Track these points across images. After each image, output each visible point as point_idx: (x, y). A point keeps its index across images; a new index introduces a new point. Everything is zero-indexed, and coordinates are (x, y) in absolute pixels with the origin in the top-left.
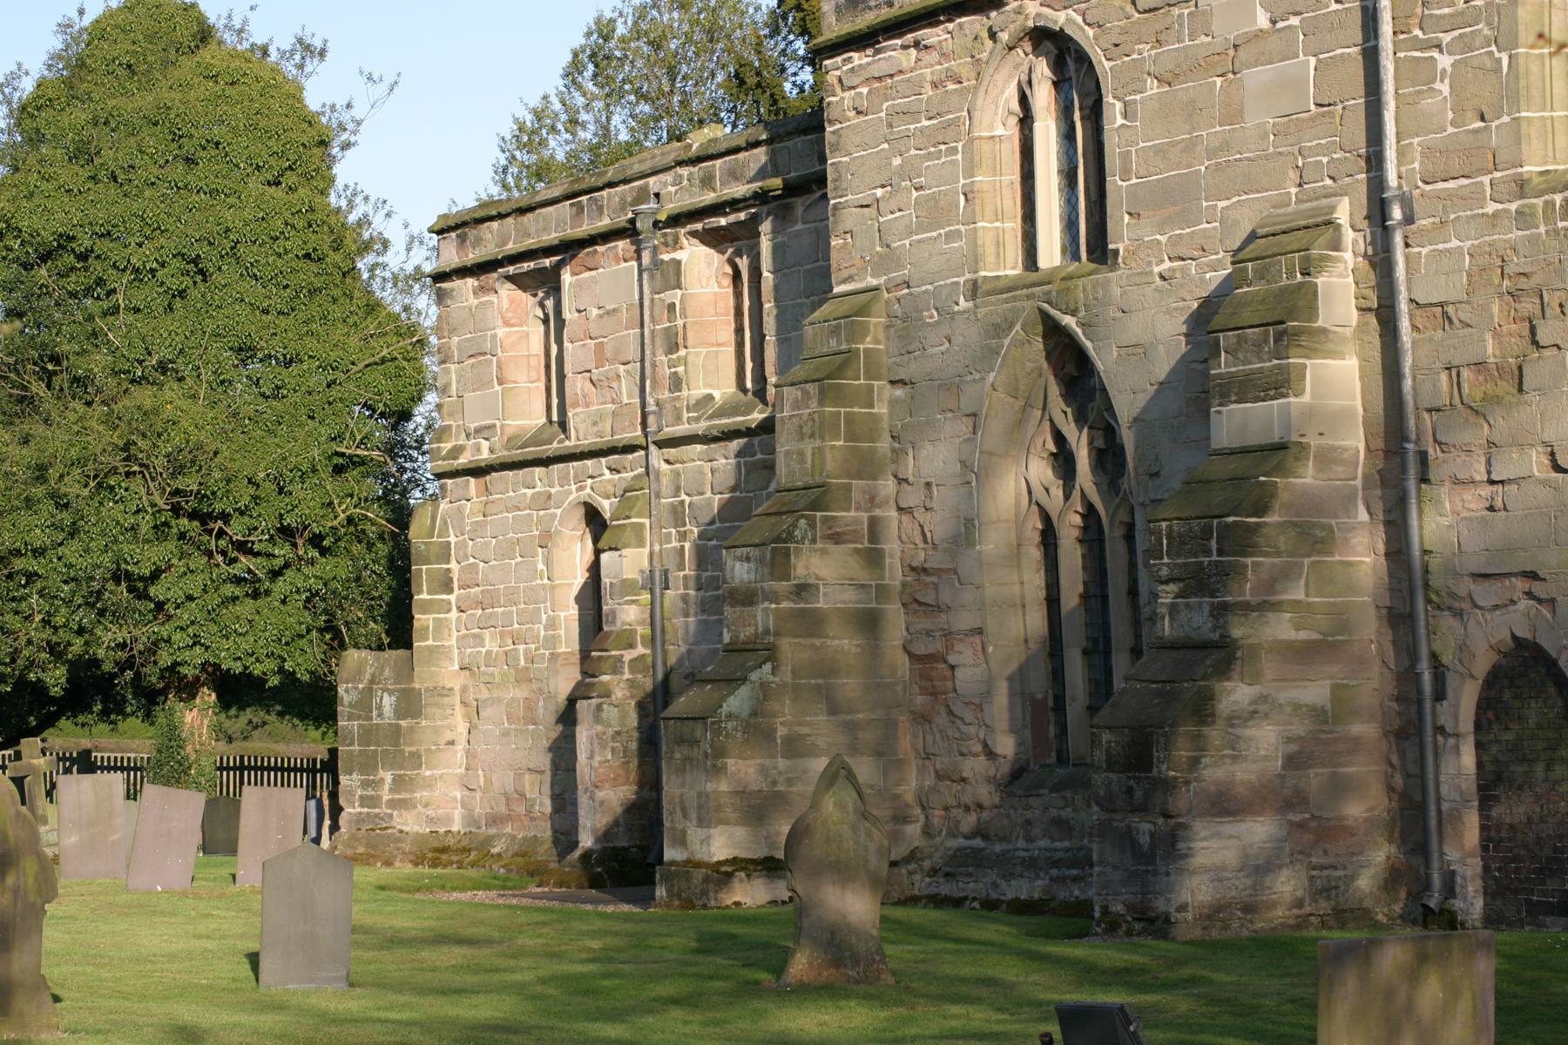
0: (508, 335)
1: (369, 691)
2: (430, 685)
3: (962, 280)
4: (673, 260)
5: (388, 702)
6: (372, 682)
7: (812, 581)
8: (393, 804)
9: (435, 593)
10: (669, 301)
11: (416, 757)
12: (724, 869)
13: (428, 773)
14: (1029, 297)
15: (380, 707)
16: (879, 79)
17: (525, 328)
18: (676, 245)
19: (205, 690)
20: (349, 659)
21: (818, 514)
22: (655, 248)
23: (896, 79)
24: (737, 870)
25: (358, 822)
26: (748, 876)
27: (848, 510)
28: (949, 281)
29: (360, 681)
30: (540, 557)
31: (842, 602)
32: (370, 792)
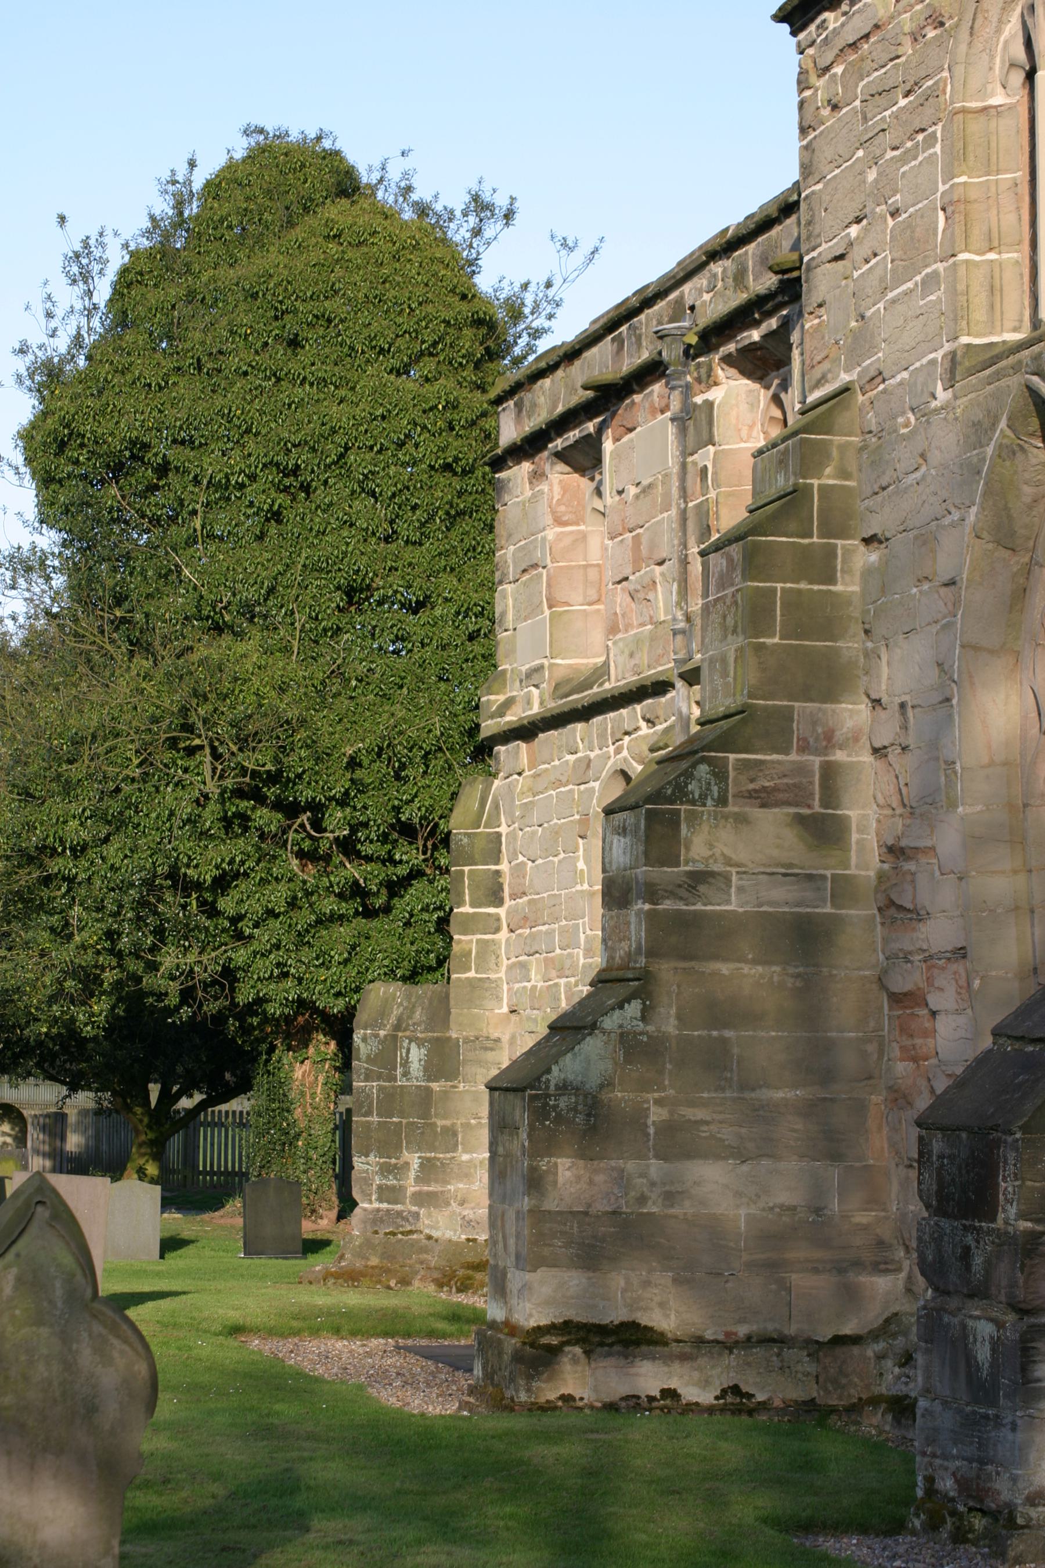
0: (559, 537)
1: (392, 1041)
2: (471, 1034)
3: (939, 355)
4: (706, 401)
5: (416, 1055)
6: (397, 1027)
7: (716, 868)
8: (421, 1199)
9: (480, 906)
10: (701, 465)
11: (451, 1132)
12: (545, 1340)
13: (465, 1157)
14: (1016, 368)
15: (406, 1063)
16: (853, 46)
17: (582, 527)
18: (709, 381)
19: (321, 1037)
20: (372, 995)
21: (732, 757)
22: (688, 386)
23: (872, 40)
24: (568, 1343)
25: (374, 1222)
26: (588, 1353)
27: (786, 751)
28: (924, 361)
29: (382, 1026)
30: (581, 852)
31: (770, 903)
32: (392, 1182)
